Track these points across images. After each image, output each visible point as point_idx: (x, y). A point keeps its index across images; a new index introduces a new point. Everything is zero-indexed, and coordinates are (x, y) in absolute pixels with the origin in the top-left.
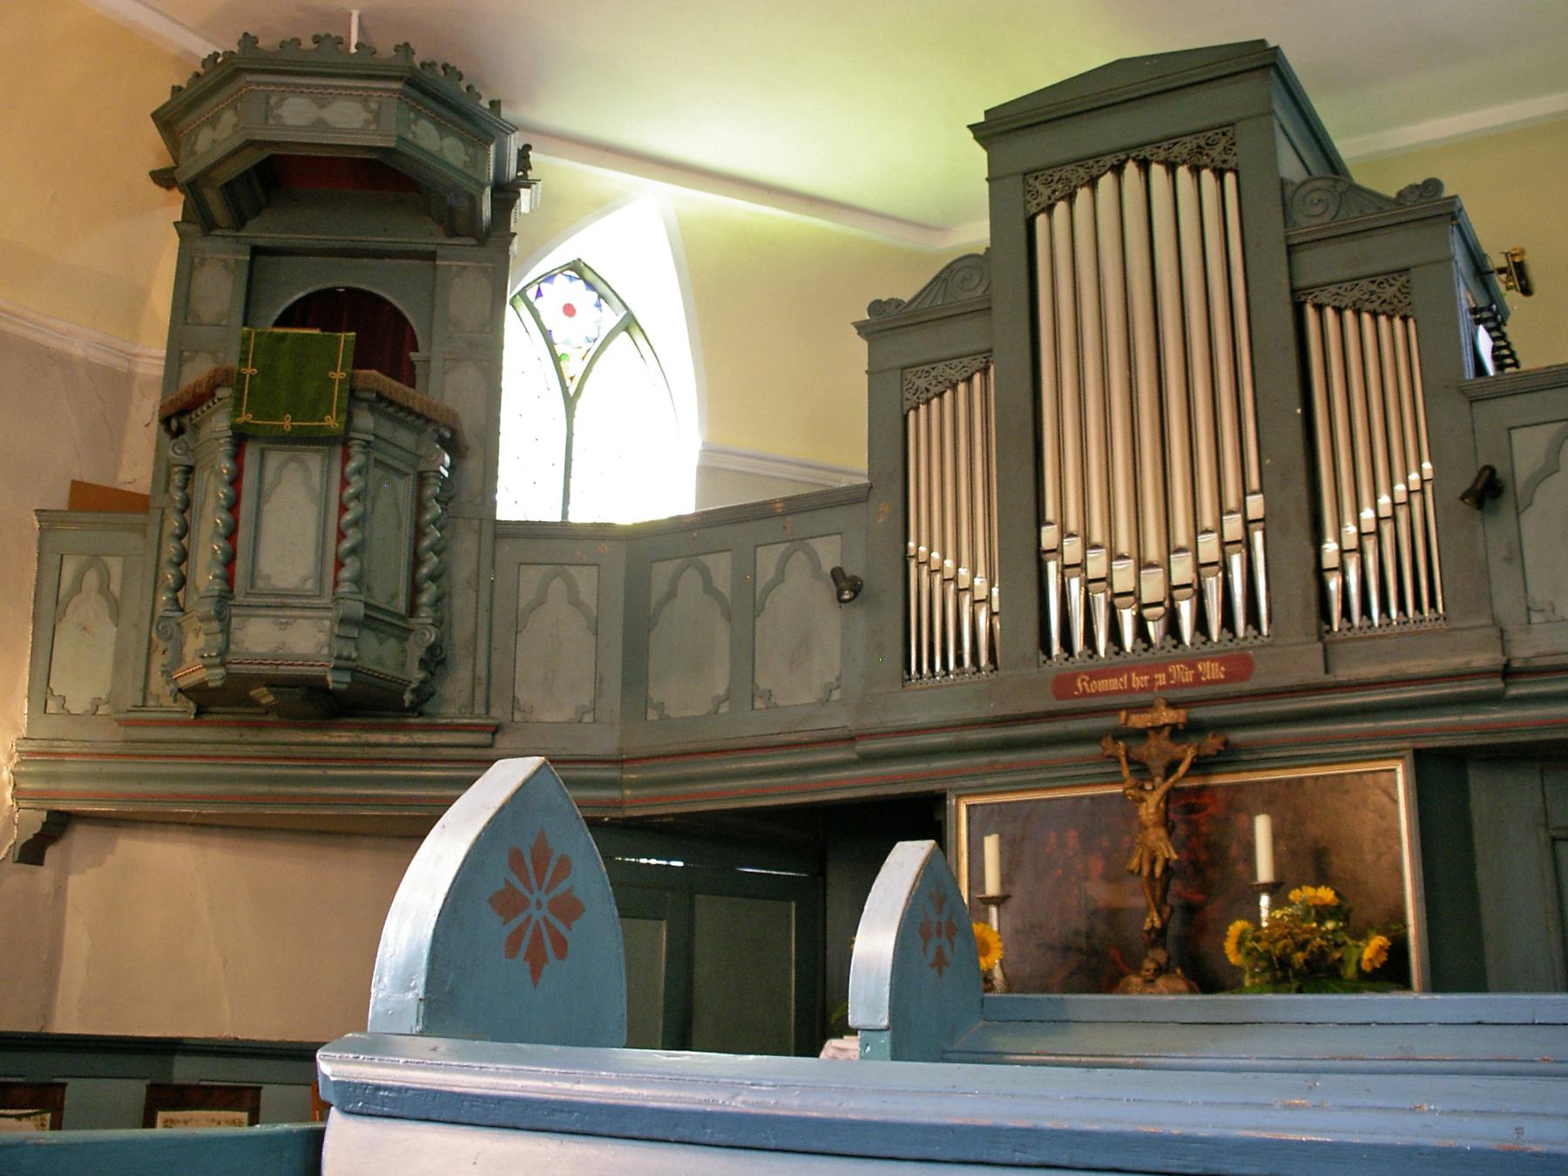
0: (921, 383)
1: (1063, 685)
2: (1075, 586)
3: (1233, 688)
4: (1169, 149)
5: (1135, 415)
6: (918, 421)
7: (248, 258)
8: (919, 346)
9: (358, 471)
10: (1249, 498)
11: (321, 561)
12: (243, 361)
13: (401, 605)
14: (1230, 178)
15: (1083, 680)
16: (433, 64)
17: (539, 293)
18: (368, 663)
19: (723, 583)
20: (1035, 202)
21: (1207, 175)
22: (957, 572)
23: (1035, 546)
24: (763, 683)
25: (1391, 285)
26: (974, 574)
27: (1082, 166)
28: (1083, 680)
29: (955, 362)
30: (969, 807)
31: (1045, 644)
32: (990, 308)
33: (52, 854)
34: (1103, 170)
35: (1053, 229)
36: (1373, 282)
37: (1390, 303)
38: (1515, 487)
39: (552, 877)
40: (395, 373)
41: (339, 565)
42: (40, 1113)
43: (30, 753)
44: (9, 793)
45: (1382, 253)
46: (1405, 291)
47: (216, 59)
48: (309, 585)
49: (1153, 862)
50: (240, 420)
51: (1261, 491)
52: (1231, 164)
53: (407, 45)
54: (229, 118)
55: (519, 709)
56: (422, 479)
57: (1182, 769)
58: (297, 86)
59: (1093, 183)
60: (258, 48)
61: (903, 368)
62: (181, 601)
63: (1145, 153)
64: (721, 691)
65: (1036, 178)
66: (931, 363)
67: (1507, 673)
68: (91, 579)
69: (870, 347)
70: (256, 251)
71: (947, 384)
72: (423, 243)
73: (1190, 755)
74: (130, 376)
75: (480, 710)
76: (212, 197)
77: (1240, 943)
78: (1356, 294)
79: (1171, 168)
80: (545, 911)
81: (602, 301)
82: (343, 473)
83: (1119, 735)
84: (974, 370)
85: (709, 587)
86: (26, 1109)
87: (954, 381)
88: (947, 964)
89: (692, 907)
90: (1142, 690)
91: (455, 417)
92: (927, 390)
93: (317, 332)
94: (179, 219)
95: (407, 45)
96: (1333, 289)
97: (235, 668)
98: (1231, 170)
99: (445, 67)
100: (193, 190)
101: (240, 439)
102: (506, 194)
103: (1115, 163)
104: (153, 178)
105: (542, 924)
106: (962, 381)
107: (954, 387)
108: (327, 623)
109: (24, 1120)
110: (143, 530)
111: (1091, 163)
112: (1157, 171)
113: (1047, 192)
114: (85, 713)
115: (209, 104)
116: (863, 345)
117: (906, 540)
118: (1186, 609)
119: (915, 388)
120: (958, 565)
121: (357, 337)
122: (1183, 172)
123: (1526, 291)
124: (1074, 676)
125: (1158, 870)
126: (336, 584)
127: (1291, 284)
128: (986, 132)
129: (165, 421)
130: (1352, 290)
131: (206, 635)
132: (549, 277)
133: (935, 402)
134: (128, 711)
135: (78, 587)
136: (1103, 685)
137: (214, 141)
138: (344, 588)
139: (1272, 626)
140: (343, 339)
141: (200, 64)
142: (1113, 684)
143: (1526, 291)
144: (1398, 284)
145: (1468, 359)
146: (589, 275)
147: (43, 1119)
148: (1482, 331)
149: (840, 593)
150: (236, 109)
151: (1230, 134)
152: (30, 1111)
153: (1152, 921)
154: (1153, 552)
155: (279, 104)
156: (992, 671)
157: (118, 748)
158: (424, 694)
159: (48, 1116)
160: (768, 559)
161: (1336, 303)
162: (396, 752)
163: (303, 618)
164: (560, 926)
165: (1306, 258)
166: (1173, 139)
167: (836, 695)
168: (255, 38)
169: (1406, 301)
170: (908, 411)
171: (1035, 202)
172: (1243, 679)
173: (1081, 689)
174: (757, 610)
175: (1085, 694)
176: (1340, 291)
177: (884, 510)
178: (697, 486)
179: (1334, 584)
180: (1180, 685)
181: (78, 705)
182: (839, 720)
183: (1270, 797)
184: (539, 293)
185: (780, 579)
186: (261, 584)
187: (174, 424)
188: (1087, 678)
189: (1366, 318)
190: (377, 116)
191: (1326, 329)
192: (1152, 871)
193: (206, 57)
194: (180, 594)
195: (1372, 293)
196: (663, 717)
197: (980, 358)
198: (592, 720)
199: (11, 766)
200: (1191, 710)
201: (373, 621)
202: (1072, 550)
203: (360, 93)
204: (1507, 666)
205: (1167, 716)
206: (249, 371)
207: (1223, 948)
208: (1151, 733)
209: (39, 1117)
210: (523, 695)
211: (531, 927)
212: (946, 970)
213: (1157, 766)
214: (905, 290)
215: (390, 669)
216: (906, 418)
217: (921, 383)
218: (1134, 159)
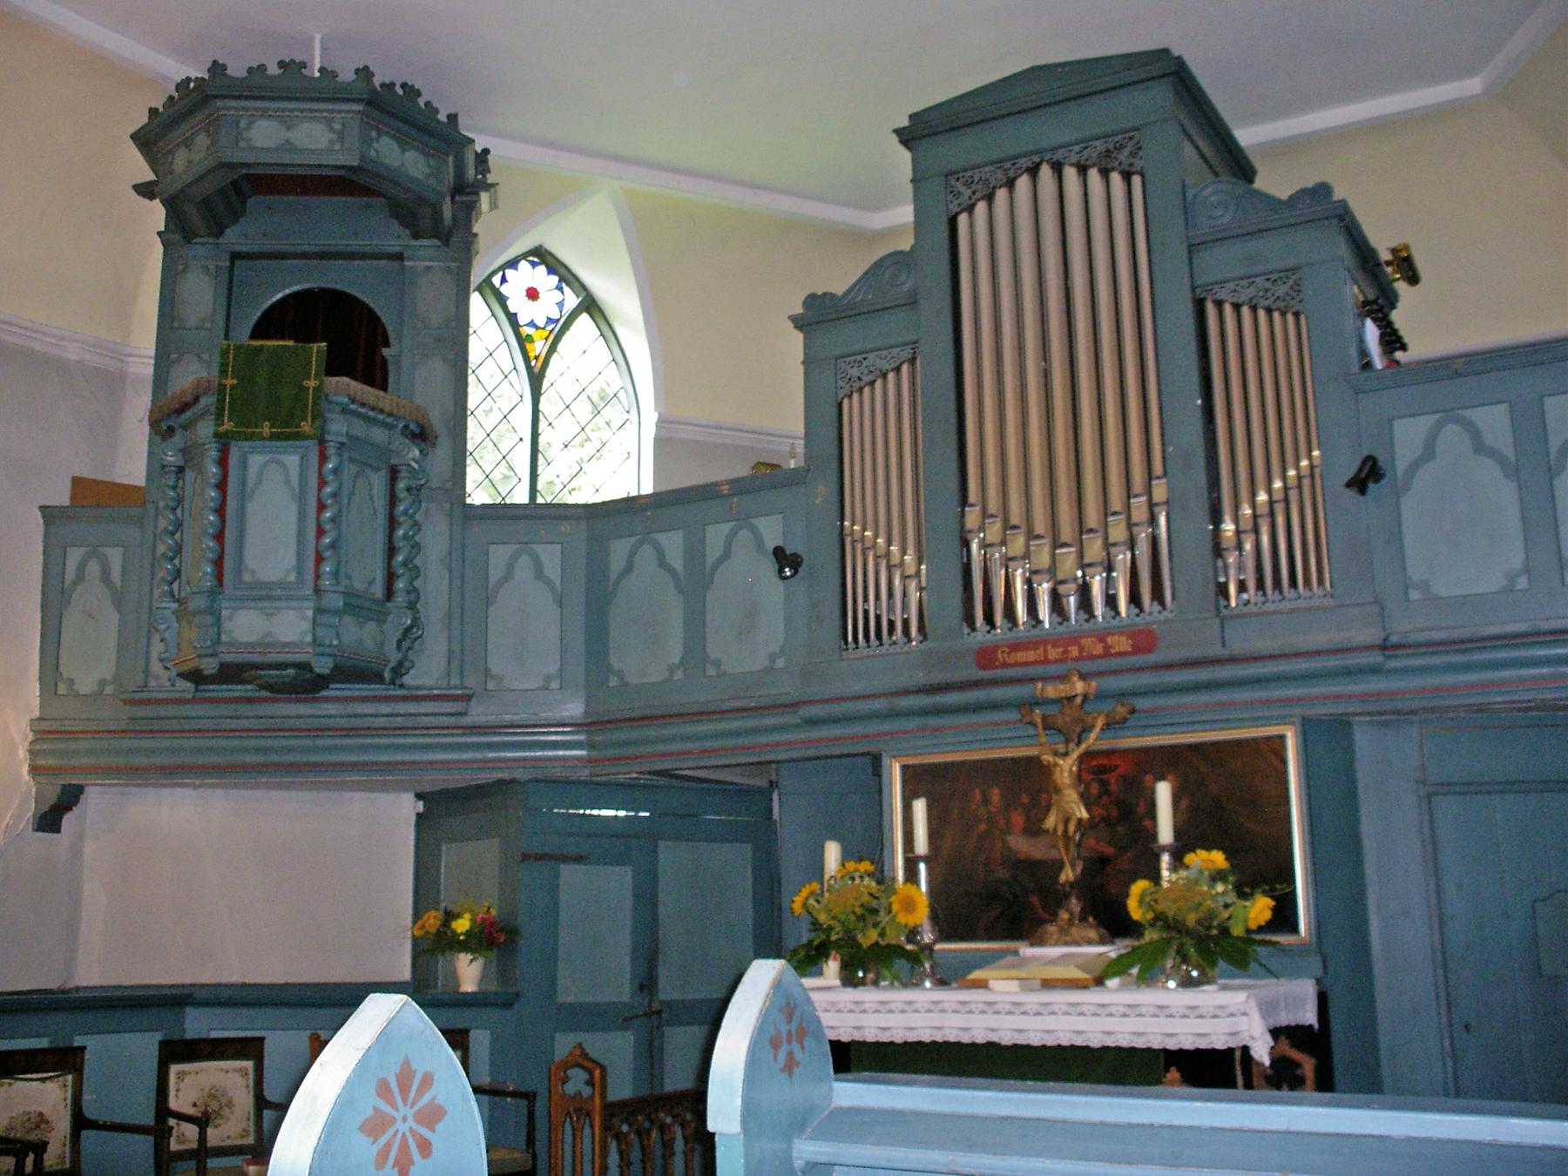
0: (854, 372)
4: (1080, 152)
6: (851, 408)
7: (228, 264)
8: (847, 336)
9: (335, 471)
10: (1154, 482)
11: (300, 555)
12: (223, 372)
13: (378, 590)
14: (1136, 180)
15: (1003, 652)
16: (393, 85)
17: (504, 280)
19: (676, 558)
20: (957, 202)
21: (1116, 177)
25: (1285, 283)
26: (904, 552)
27: (999, 168)
28: (1003, 652)
29: (885, 352)
31: (969, 619)
32: (916, 302)
33: (68, 820)
34: (1020, 172)
35: (974, 227)
36: (1268, 280)
37: (1284, 300)
39: (417, 1091)
40: (369, 380)
41: (319, 559)
42: (60, 1076)
43: (44, 732)
44: (25, 769)
45: (1275, 251)
46: (1297, 289)
47: (189, 84)
48: (292, 578)
49: (1066, 821)
50: (221, 429)
51: (1165, 474)
53: (366, 68)
54: (202, 140)
55: (492, 678)
58: (265, 110)
59: (1010, 184)
60: (226, 75)
61: (836, 359)
62: (176, 593)
63: (1058, 156)
64: (676, 659)
65: (958, 179)
66: (863, 353)
68: (93, 568)
69: (805, 339)
70: (235, 256)
71: (878, 373)
72: (394, 245)
74: (123, 375)
75: (455, 681)
76: (191, 211)
77: (1141, 902)
78: (1252, 291)
80: (411, 1123)
81: (564, 285)
82: (320, 473)
84: (902, 360)
85: (662, 563)
86: (49, 1072)
87: (884, 371)
88: (798, 1064)
89: (655, 851)
90: (1056, 661)
92: (860, 379)
93: (291, 343)
94: (163, 229)
95: (366, 68)
96: (1231, 286)
97: (229, 658)
98: (1137, 173)
99: (404, 86)
100: (171, 204)
101: (224, 442)
103: (1031, 165)
105: (408, 1135)
106: (892, 370)
107: (884, 376)
109: (48, 1082)
110: (140, 523)
111: (1008, 165)
113: (968, 193)
114: (93, 694)
115: (185, 126)
116: (798, 337)
117: (842, 519)
119: (848, 376)
120: (889, 542)
121: (328, 346)
122: (1094, 175)
123: (1413, 279)
124: (995, 648)
125: (1072, 828)
126: (317, 576)
127: (1192, 282)
128: (907, 137)
129: (154, 424)
130: (1248, 287)
131: (198, 627)
132: (513, 264)
133: (867, 390)
134: (134, 691)
135: (80, 577)
136: (1021, 656)
137: (190, 162)
140: (315, 350)
141: (174, 87)
142: (1031, 655)
143: (1413, 279)
144: (1291, 282)
145: (1353, 352)
147: (65, 1081)
148: (1369, 324)
149: (781, 571)
150: (208, 131)
151: (1136, 139)
152: (52, 1074)
153: (1067, 876)
154: (1067, 530)
155: (249, 127)
156: (921, 642)
157: (122, 726)
158: (399, 671)
159: (70, 1077)
160: (716, 536)
161: (1234, 300)
162: (381, 722)
163: (288, 608)
164: (424, 1132)
165: (1206, 259)
166: (1085, 142)
167: (780, 663)
168: (224, 65)
169: (1298, 299)
170: (843, 399)
171: (957, 202)
172: (1150, 650)
173: (1001, 660)
175: (1005, 665)
176: (1238, 288)
177: (822, 492)
180: (1092, 657)
181: (86, 686)
182: (790, 689)
184: (504, 280)
185: (726, 555)
186: (247, 577)
188: (1007, 650)
189: (1262, 314)
190: (341, 137)
191: (1223, 326)
192: (1066, 831)
193: (179, 80)
194: (176, 586)
195: (1267, 290)
196: (624, 684)
197: (908, 349)
198: (558, 687)
199: (27, 744)
201: (355, 606)
203: (324, 114)
204: (1385, 640)
206: (230, 382)
207: (1125, 906)
209: (61, 1079)
210: (495, 666)
211: (399, 1136)
212: (796, 1070)
216: (840, 405)
218: (1048, 161)
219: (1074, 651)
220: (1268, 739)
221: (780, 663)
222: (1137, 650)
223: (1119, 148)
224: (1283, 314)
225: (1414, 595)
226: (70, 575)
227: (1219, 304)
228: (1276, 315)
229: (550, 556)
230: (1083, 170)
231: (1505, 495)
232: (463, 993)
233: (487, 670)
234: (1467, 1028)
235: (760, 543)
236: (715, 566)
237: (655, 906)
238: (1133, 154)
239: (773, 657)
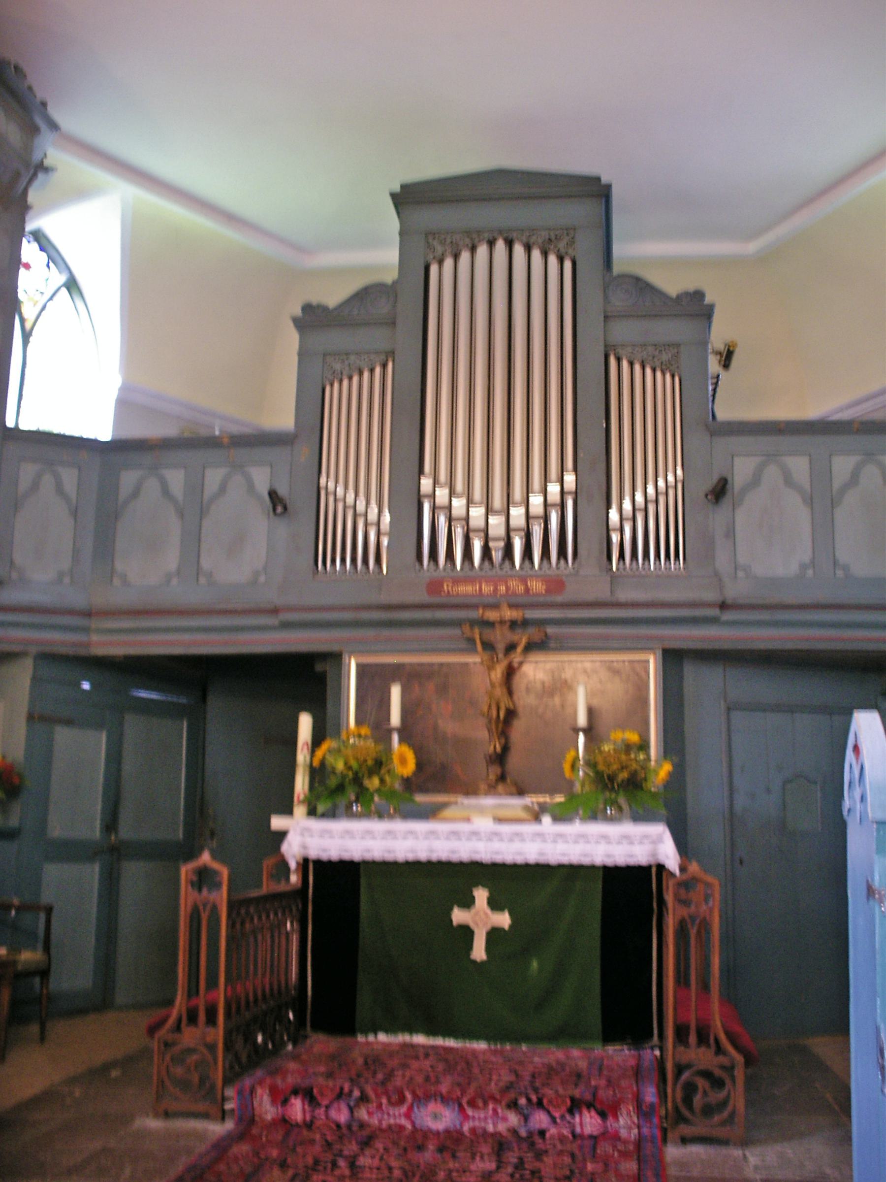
1: (434, 586)
2: (442, 521)
3: (550, 599)
5: (491, 410)
6: (333, 393)
8: (337, 339)
22: (451, 501)
23: (417, 493)
38: (733, 488)
46: (677, 356)
67: (723, 606)
73: (524, 641)
81: (51, 264)
89: (121, 724)
99: (16, 68)
118: (518, 545)
122: (536, 254)
125: (502, 715)
136: (462, 589)
139: (576, 562)
146: (44, 242)
149: (274, 510)
154: (498, 502)
160: (214, 477)
166: (533, 230)
173: (446, 590)
174: (203, 512)
177: (304, 453)
178: (115, 411)
179: (615, 538)
180: (515, 594)
182: (270, 596)
200: (526, 612)
202: (442, 494)
205: (509, 614)
208: (497, 625)
210: (18, 558)
213: (501, 647)
217: (338, 366)
219: (503, 588)
227: (619, 360)
230: (528, 249)
231: (803, 515)
233: (12, 562)
234: (741, 862)
235: (251, 487)
237: (119, 763)
239: (256, 574)
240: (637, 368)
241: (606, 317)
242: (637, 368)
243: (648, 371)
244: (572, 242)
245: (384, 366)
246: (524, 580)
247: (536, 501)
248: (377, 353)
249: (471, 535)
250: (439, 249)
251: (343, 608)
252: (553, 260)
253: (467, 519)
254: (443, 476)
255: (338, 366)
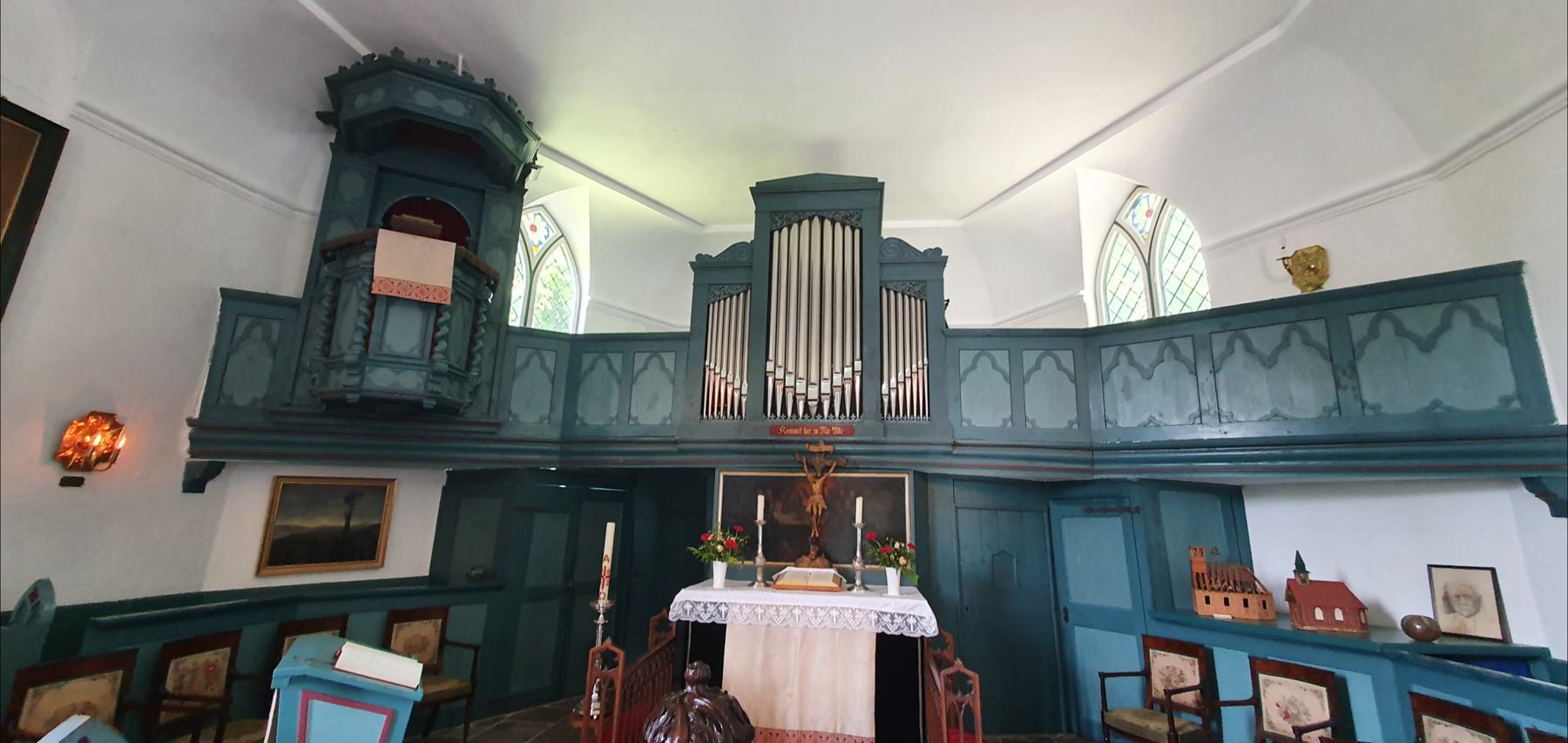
1: (774, 430)
6: (714, 309)
11: (423, 340)
18: (445, 395)
24: (634, 413)
30: (724, 476)
41: (434, 343)
46: (924, 288)
52: (860, 225)
56: (478, 302)
57: (831, 470)
59: (800, 223)
63: (825, 214)
78: (904, 287)
79: (833, 223)
83: (801, 452)
91: (498, 275)
95: (492, 80)
96: (895, 283)
102: (528, 169)
104: (318, 117)
107: (731, 297)
108: (425, 373)
112: (827, 223)
122: (838, 226)
136: (791, 431)
138: (436, 356)
142: (796, 431)
154: (814, 378)
166: (837, 211)
172: (851, 435)
179: (886, 400)
183: (860, 487)
187: (329, 254)
214: (715, 251)
215: (454, 398)
217: (717, 293)
219: (816, 431)
220: (196, 457)
221: (669, 422)
222: (844, 434)
223: (851, 216)
224: (916, 299)
225: (964, 424)
226: (239, 333)
228: (913, 299)
229: (550, 359)
232: (1133, 604)
233: (510, 411)
234: (967, 609)
236: (586, 373)
238: (858, 220)
240: (900, 295)
241: (881, 264)
242: (900, 295)
243: (906, 297)
244: (859, 219)
245: (745, 293)
246: (829, 427)
247: (837, 379)
248: (742, 284)
249: (798, 397)
250: (780, 222)
251: (719, 442)
252: (848, 229)
253: (806, 395)
254: (780, 362)
255: (717, 293)
